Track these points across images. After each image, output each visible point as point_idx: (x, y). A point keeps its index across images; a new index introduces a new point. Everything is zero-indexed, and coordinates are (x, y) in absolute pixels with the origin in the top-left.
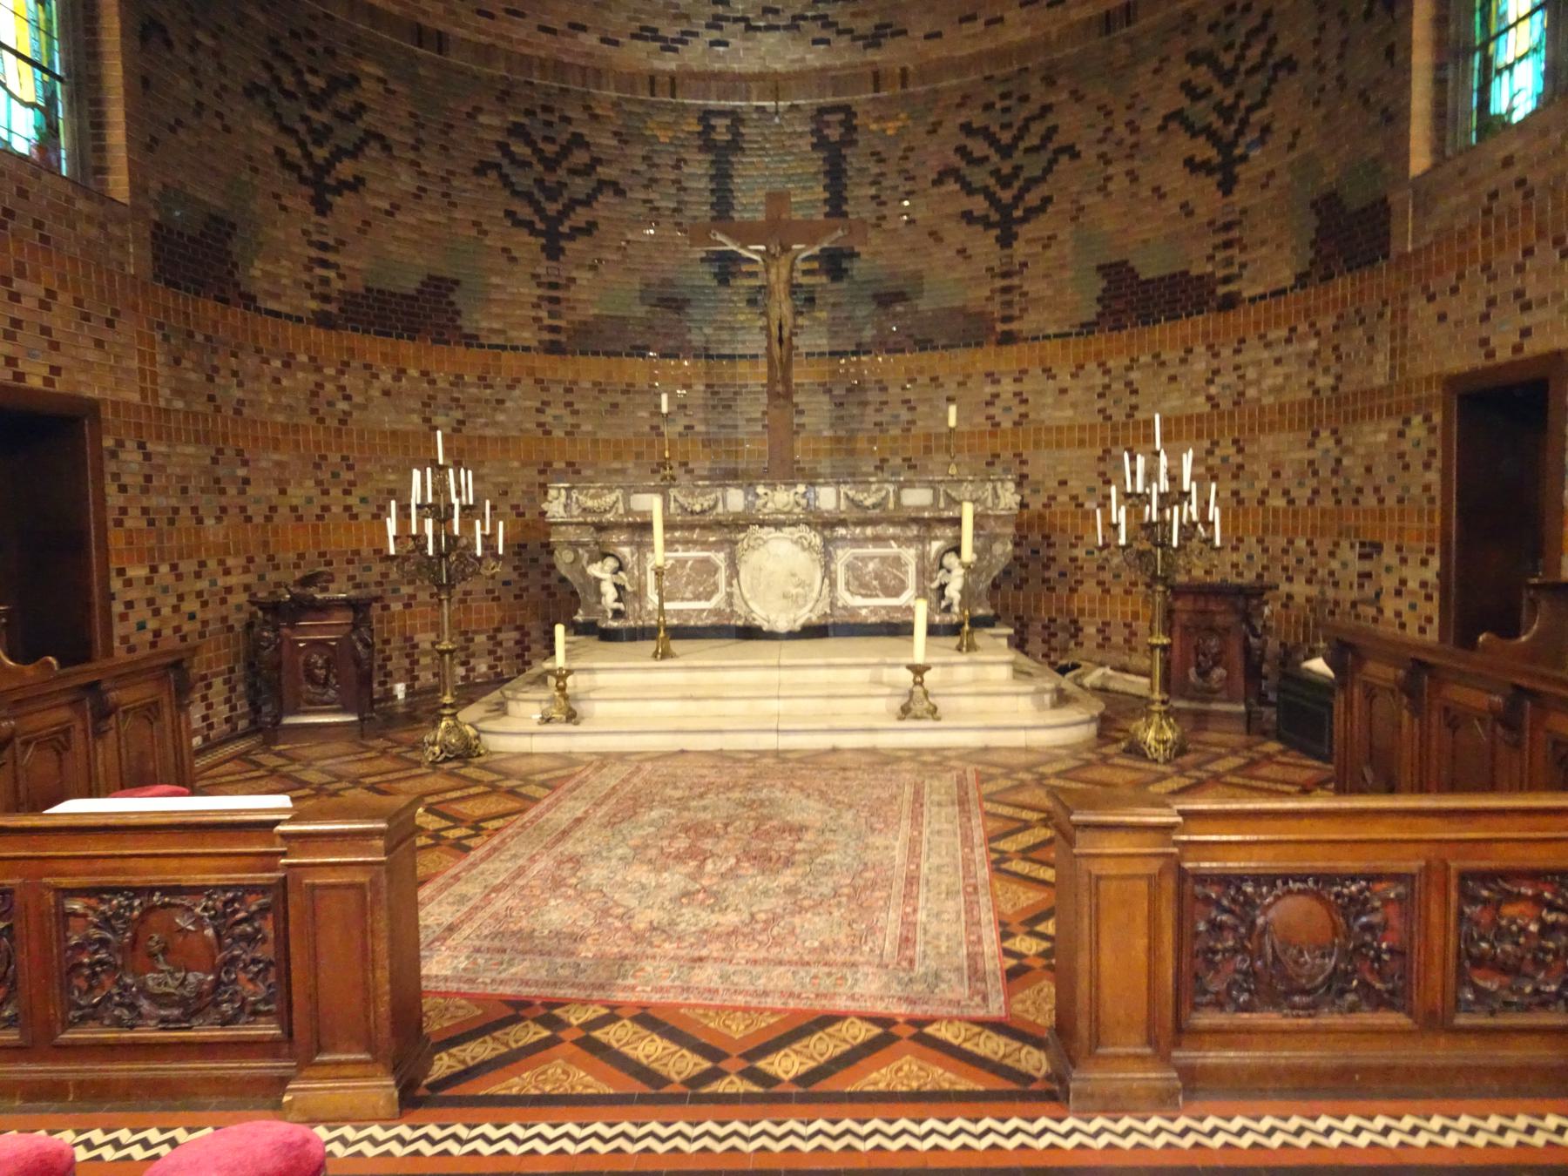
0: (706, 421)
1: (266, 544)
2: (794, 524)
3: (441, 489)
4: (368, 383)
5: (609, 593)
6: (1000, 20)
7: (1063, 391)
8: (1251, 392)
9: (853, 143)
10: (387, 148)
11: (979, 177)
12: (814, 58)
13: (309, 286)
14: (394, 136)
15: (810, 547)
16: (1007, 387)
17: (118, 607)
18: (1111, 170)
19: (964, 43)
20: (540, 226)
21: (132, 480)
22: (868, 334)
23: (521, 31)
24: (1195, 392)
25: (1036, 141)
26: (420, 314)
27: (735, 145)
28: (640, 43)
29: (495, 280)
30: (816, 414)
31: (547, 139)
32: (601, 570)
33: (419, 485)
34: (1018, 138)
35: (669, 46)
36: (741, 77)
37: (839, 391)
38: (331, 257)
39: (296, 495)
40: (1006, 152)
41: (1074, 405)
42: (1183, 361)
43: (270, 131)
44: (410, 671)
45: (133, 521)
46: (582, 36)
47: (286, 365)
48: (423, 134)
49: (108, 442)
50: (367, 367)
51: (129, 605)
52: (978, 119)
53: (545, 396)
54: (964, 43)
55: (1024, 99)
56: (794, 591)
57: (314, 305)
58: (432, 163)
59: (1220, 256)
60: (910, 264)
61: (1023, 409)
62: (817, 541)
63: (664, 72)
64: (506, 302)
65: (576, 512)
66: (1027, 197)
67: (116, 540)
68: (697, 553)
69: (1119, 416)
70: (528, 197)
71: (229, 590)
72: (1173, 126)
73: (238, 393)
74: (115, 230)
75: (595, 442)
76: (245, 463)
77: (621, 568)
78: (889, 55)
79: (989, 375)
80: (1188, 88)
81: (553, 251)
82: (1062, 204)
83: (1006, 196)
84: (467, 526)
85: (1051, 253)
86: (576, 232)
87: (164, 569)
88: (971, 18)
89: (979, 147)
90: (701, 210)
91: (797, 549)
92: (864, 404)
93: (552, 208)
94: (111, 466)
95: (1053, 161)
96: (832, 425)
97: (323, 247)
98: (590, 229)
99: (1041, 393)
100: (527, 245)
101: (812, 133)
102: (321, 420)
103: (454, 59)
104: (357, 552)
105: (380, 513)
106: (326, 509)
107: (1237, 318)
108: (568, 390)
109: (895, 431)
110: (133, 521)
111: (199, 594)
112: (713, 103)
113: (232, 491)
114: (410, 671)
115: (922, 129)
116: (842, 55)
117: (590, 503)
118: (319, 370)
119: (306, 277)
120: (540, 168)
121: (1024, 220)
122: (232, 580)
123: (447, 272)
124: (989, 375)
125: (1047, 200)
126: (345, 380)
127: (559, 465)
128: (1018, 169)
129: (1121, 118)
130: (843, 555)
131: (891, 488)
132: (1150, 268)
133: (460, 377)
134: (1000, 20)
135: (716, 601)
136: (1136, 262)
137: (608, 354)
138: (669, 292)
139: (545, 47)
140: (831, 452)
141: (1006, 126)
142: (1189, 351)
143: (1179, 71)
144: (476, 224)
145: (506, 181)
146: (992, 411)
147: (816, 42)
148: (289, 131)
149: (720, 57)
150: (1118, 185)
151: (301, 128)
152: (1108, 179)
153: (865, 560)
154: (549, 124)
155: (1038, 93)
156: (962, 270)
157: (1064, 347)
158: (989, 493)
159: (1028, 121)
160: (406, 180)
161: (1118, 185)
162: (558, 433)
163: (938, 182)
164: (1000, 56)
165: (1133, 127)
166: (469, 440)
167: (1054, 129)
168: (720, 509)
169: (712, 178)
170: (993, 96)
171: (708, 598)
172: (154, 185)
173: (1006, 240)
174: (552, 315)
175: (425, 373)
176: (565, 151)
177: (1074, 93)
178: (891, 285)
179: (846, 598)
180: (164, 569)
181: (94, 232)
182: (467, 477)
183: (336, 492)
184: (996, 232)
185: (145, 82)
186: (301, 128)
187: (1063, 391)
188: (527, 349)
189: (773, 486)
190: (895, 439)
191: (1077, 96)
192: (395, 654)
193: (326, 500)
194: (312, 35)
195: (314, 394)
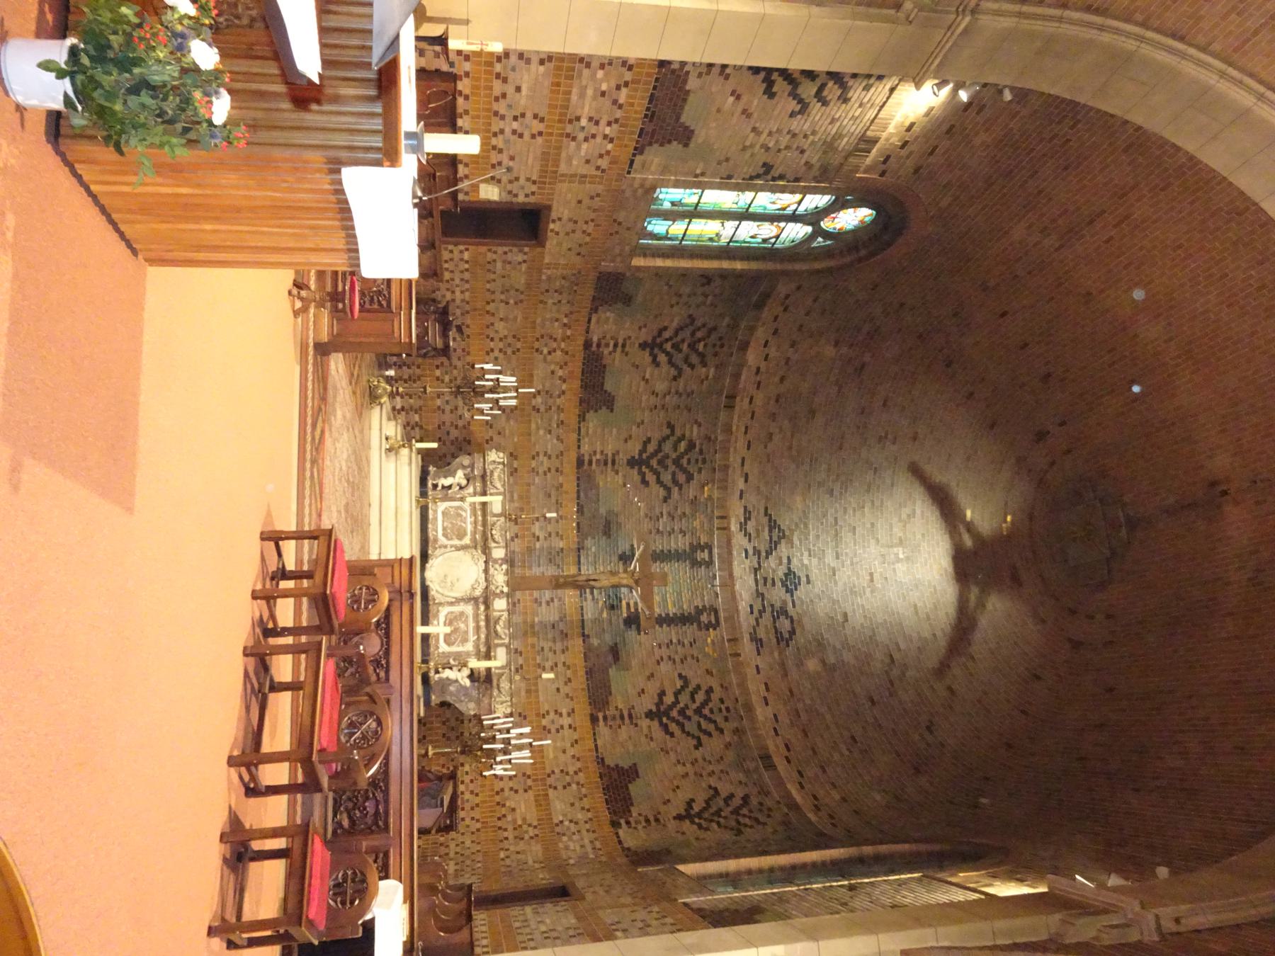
0: (542, 549)
1: (475, 310)
2: (486, 580)
3: (506, 389)
4: (557, 363)
5: (447, 482)
6: (767, 704)
7: (564, 752)
8: (565, 839)
9: (700, 629)
10: (675, 378)
11: (684, 699)
12: (743, 606)
13: (604, 337)
14: (681, 382)
15: (474, 589)
16: (566, 721)
17: (450, 247)
18: (688, 765)
19: (755, 687)
20: (644, 456)
21: (509, 257)
22: (595, 642)
23: (741, 444)
24: (565, 815)
25: (704, 727)
26: (594, 391)
27: (695, 564)
28: (742, 510)
29: (615, 430)
30: (547, 614)
31: (689, 460)
32: (459, 477)
33: (508, 380)
34: (705, 717)
35: (743, 526)
36: (730, 564)
37: (562, 626)
38: (619, 349)
39: (500, 326)
40: (698, 711)
41: (556, 758)
42: (583, 808)
43: (675, 324)
44: (401, 378)
45: (490, 256)
46: (743, 480)
47: (565, 325)
48: (684, 397)
49: (526, 249)
50: (566, 364)
51: (451, 252)
52: (715, 697)
53: (554, 457)
54: (755, 687)
55: (726, 719)
56: (449, 580)
57: (595, 339)
58: (671, 400)
59: (642, 819)
60: (634, 663)
61: (553, 731)
62: (478, 593)
63: (729, 523)
64: (603, 436)
65: (491, 467)
66: (674, 725)
67: (483, 249)
68: (469, 528)
69: (550, 781)
70: (659, 450)
71: (453, 292)
72: (712, 792)
73: (550, 301)
74: (619, 259)
75: (529, 485)
76: (516, 303)
77: (461, 488)
78: (747, 647)
79: (573, 711)
80: (732, 796)
81: (632, 463)
82: (670, 743)
83: (674, 713)
84: (488, 401)
85: (643, 739)
86: (643, 475)
87: (467, 266)
88: (767, 689)
89: (700, 697)
90: (659, 544)
91: (473, 581)
92: (554, 641)
93: (654, 462)
94: (515, 249)
95: (693, 737)
96: (541, 622)
97: (624, 346)
98: (645, 482)
99: (563, 739)
100: (634, 448)
101: (704, 606)
102: (538, 340)
103: (723, 415)
104: (468, 353)
105: (496, 361)
106: (492, 340)
107: (608, 829)
108: (557, 471)
109: (538, 660)
110: (490, 256)
111: (453, 280)
112: (716, 551)
113: (503, 297)
114: (401, 378)
115: (709, 666)
116: (745, 621)
117: (496, 474)
118: (563, 340)
119: (608, 337)
120: (674, 456)
121: (661, 723)
122: (458, 293)
123: (618, 404)
124: (573, 711)
125: (672, 735)
126: (559, 353)
127: (515, 464)
128: (689, 718)
129: (717, 768)
130: (469, 609)
131: (507, 641)
132: (635, 789)
133: (562, 411)
134: (767, 704)
135: (442, 540)
136: (639, 782)
137: (578, 492)
138: (614, 527)
139: (734, 460)
140: (525, 622)
141: (711, 711)
142: (588, 810)
143: (740, 793)
144: (643, 422)
145: (664, 439)
146: (552, 714)
147: (751, 606)
148: (676, 334)
149: (739, 554)
150: (680, 769)
151: (679, 338)
152: (684, 765)
153: (466, 622)
154: (697, 461)
155: (728, 727)
156: (632, 692)
157: (590, 750)
158: (503, 698)
159: (715, 722)
160: (661, 387)
161: (680, 769)
162: (534, 464)
163: (680, 676)
164: (749, 708)
165: (712, 774)
166: (529, 415)
167: (710, 735)
168: (493, 545)
169: (676, 551)
170: (728, 703)
171: (445, 535)
172: (641, 275)
173: (649, 715)
174: (598, 461)
175: (563, 392)
176: (685, 471)
177: (730, 744)
178: (623, 654)
179: (444, 612)
180: (467, 266)
181: (617, 251)
182: (513, 402)
183: (501, 345)
184: (654, 709)
185: (684, 275)
186: (679, 338)
187: (564, 752)
188: (579, 447)
189: (507, 573)
190: (535, 659)
191: (728, 746)
192: (411, 371)
193: (497, 340)
194: (722, 346)
195: (551, 337)
